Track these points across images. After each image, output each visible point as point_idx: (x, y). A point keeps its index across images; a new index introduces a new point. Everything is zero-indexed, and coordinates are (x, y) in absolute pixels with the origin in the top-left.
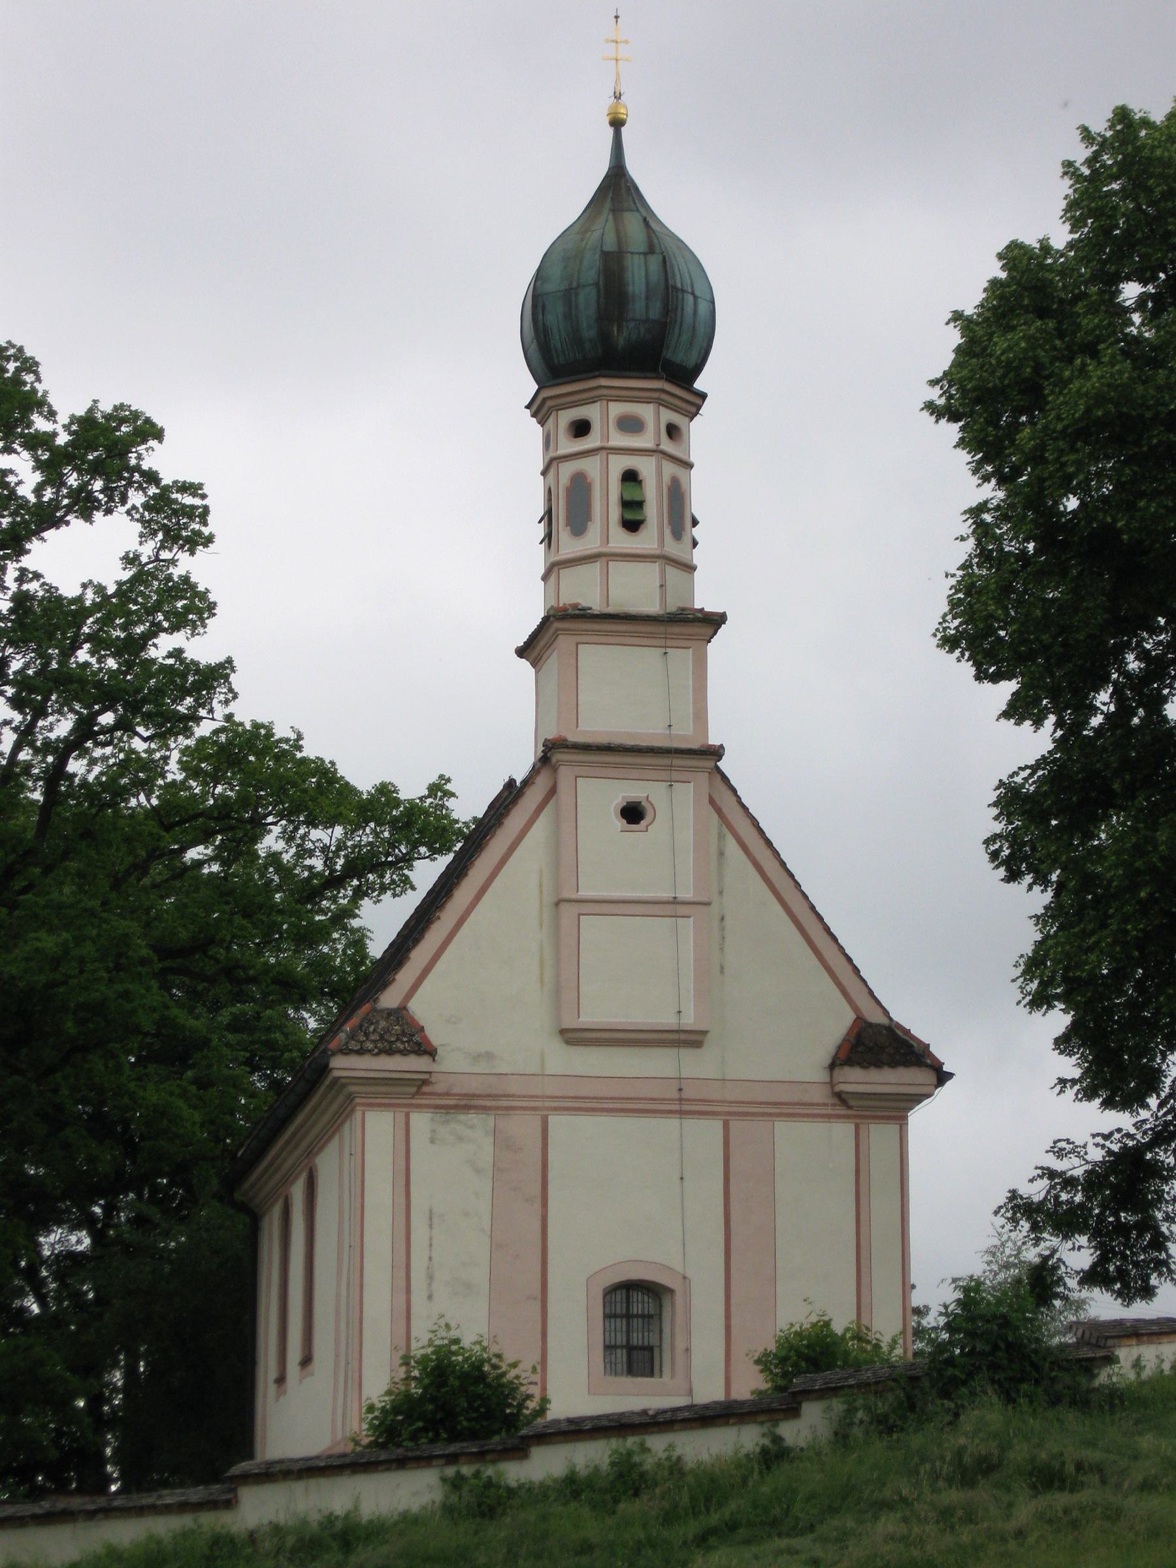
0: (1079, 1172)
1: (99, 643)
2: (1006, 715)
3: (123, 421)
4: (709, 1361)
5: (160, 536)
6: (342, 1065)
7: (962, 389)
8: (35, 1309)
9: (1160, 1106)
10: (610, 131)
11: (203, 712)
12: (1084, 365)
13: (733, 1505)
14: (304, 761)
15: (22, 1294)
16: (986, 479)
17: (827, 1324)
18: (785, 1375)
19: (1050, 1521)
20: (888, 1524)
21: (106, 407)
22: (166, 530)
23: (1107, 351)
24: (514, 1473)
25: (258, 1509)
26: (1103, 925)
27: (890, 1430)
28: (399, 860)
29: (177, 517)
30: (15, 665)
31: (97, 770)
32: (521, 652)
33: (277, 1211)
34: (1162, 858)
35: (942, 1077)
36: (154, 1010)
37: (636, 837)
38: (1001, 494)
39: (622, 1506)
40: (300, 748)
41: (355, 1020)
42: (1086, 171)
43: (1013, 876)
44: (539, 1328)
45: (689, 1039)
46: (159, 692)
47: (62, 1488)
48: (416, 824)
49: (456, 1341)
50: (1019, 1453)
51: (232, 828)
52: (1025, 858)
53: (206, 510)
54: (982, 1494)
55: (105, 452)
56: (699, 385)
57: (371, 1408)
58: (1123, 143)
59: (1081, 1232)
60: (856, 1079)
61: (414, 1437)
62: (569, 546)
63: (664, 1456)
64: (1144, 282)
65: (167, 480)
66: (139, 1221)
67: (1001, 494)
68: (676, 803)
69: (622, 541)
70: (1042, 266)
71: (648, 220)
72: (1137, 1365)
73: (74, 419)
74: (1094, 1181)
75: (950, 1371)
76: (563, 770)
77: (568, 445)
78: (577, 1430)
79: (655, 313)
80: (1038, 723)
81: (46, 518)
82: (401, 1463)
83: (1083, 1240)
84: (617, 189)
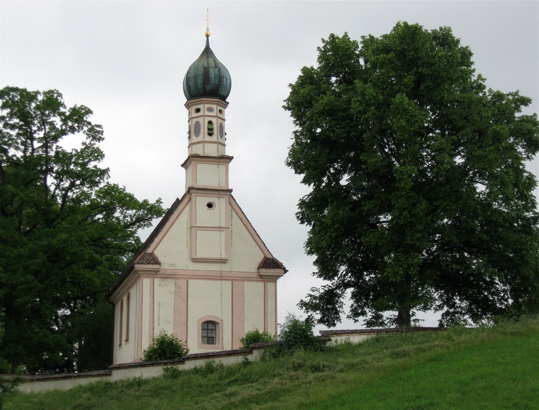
0: (318, 295)
1: (76, 164)
2: (302, 182)
3: (83, 109)
4: (227, 341)
5: (91, 138)
6: (137, 267)
7: (292, 102)
8: (57, 329)
9: (338, 279)
10: (206, 38)
11: (102, 181)
12: (322, 96)
13: (237, 375)
14: (126, 193)
15: (54, 325)
16: (297, 125)
17: (258, 331)
18: (247, 344)
19: (317, 379)
20: (276, 380)
21: (79, 106)
22: (93, 136)
23: (328, 93)
24: (181, 367)
25: (117, 376)
26: (326, 234)
27: (275, 357)
28: (149, 218)
29: (95, 133)
30: (56, 168)
31: (75, 195)
32: (182, 166)
33: (119, 303)
34: (341, 218)
35: (286, 271)
36: (89, 254)
37: (210, 211)
38: (301, 129)
39: (209, 375)
40: (125, 191)
41: (141, 256)
42: (323, 50)
43: (302, 223)
45: (223, 261)
46: (91, 176)
47: (63, 371)
48: (154, 210)
49: (166, 335)
50: (308, 363)
51: (108, 210)
52: (306, 218)
53: (103, 131)
54: (300, 372)
55: (78, 116)
56: (227, 100)
57: (145, 351)
58: (332, 43)
59: (318, 310)
60: (264, 272)
61: (156, 359)
62: (195, 139)
63: (218, 363)
64: (337, 77)
65: (93, 124)
66: (83, 307)
67: (301, 129)
68: (221, 203)
69: (208, 138)
70: (312, 73)
71: (215, 60)
72: (336, 341)
73: (71, 108)
74: (321, 297)
75: (290, 343)
76: (193, 195)
77: (194, 115)
78: (196, 357)
79: (217, 82)
80: (309, 185)
81: (63, 133)
82: (153, 365)
83: (318, 312)
84: (207, 52)
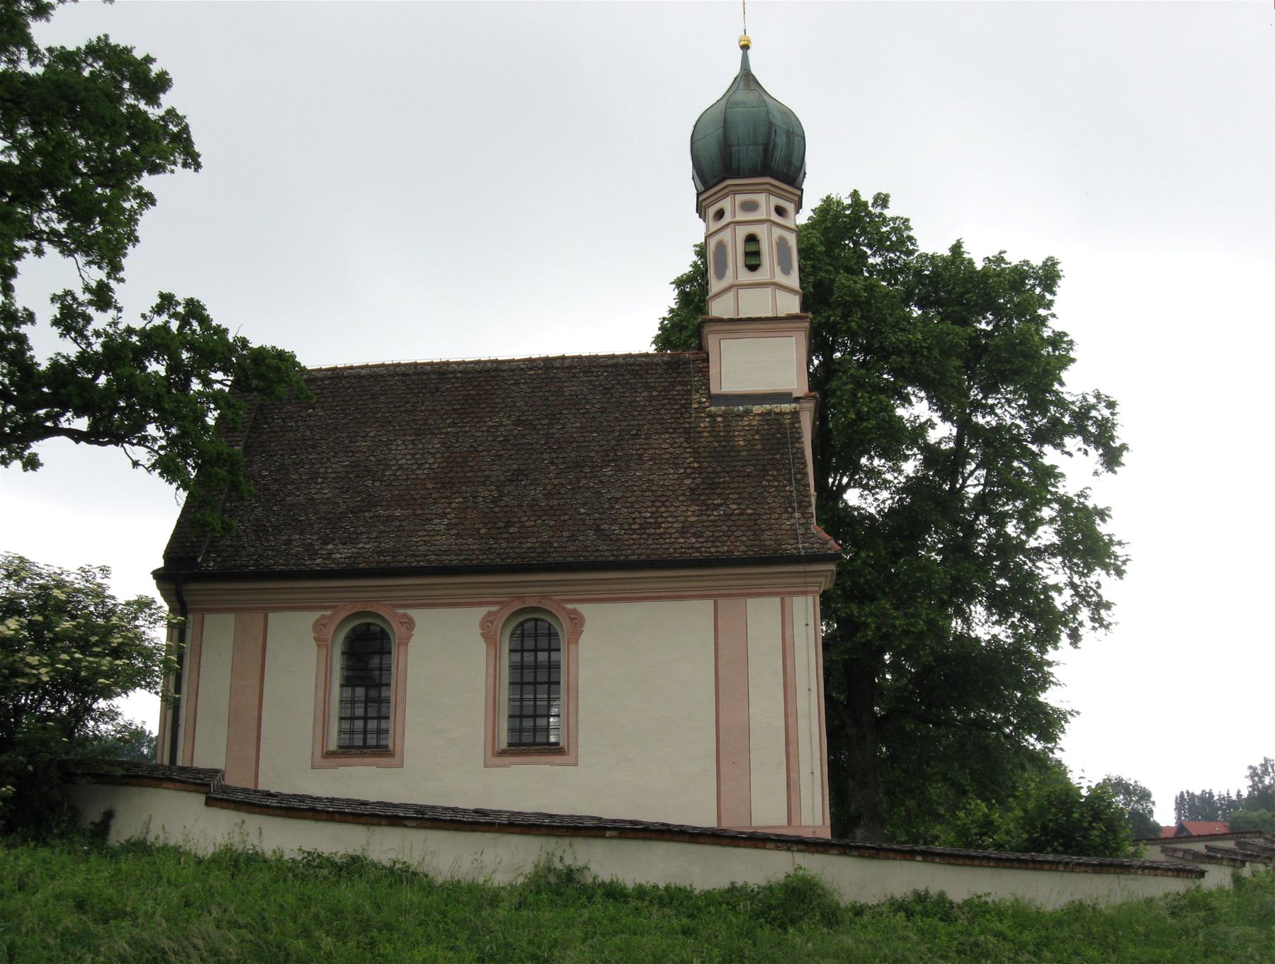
44: (720, 682)
69: (746, 277)
84: (746, 78)
